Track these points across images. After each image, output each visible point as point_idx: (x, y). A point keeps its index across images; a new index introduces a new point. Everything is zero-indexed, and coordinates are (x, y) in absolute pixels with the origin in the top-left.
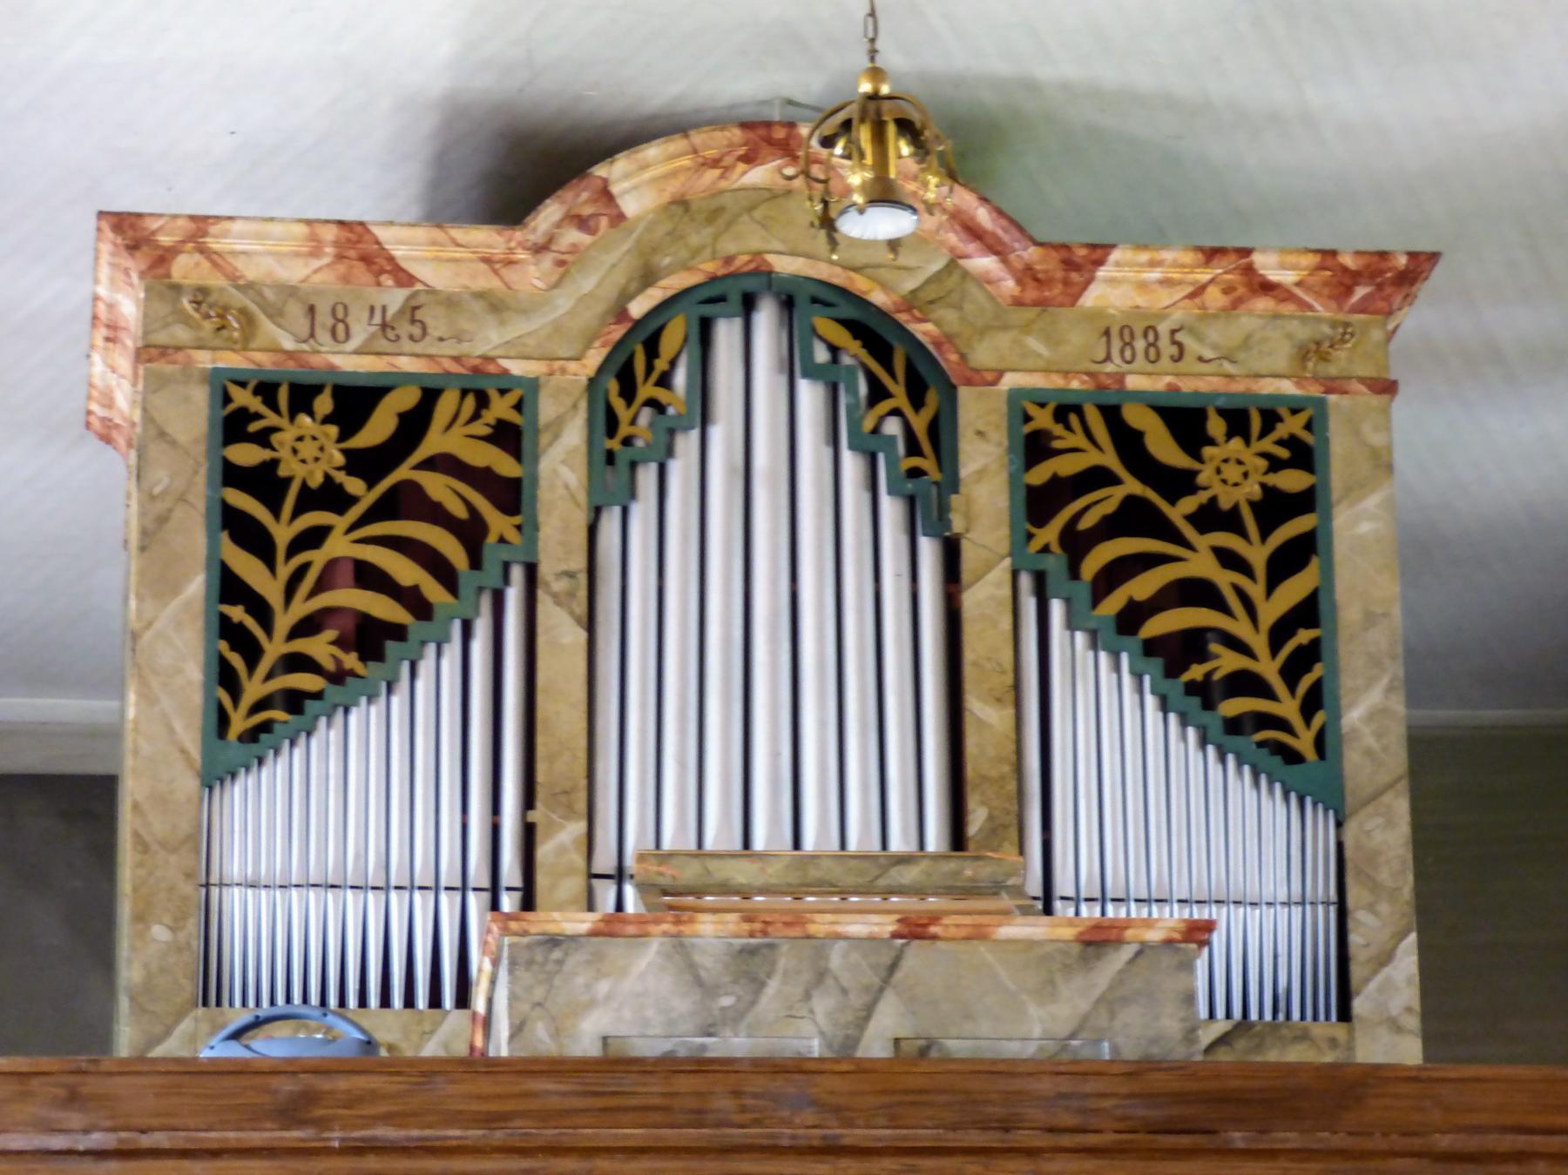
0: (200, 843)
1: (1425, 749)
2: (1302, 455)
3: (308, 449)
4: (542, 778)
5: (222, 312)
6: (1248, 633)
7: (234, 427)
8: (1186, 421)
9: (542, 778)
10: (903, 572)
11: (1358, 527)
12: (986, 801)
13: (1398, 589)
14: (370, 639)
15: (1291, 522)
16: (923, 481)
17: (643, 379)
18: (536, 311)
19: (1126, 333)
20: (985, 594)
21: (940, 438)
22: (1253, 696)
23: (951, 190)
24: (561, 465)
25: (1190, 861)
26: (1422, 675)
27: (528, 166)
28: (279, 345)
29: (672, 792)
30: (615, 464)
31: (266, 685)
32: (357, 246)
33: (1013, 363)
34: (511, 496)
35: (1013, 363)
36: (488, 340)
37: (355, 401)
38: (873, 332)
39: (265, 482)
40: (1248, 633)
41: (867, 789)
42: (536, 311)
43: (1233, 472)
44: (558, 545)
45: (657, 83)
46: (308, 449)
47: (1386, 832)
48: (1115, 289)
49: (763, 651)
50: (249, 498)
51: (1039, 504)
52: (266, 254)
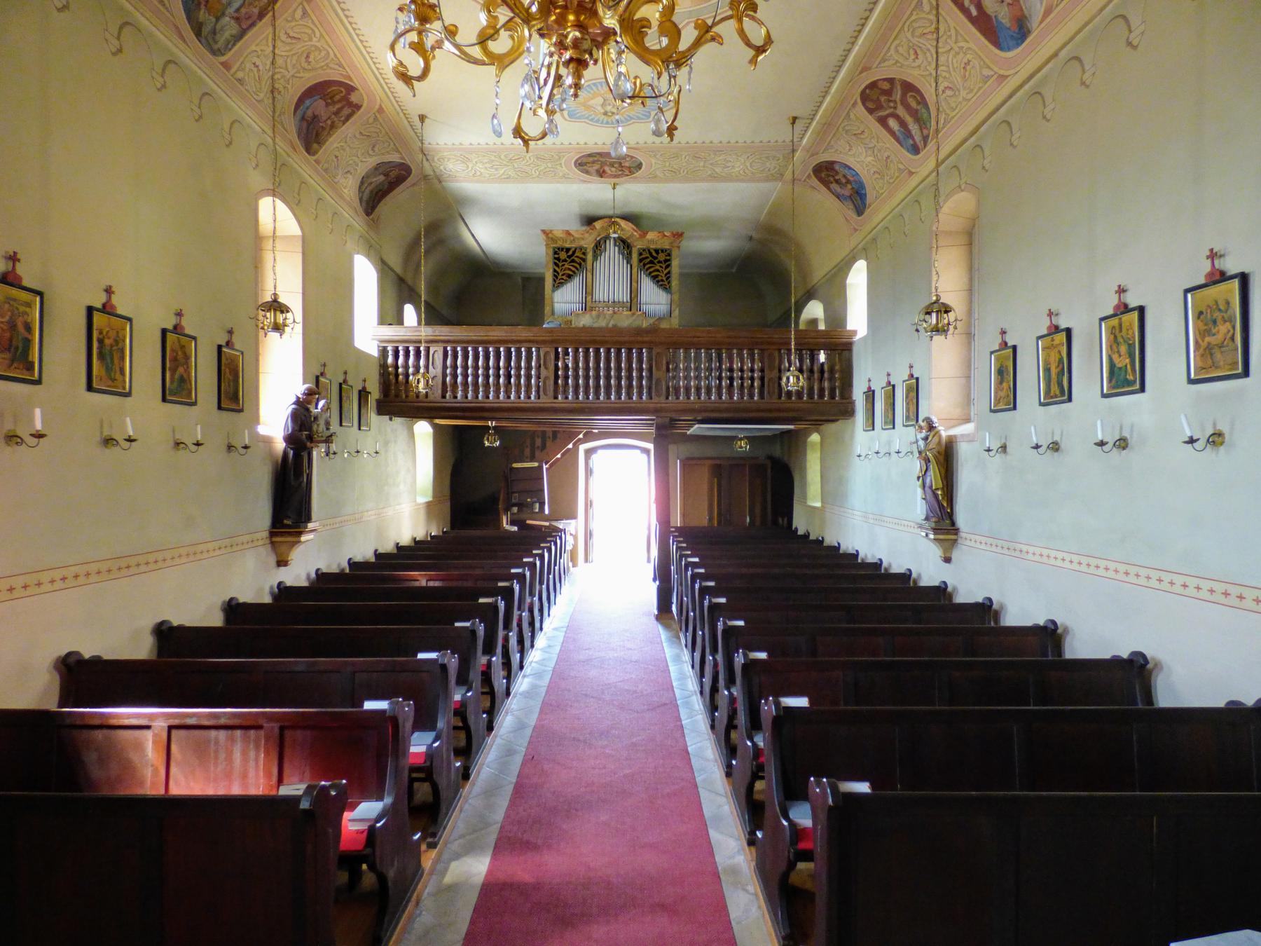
0: (552, 299)
1: (681, 275)
2: (669, 255)
3: (563, 255)
4: (588, 291)
5: (554, 240)
6: (662, 276)
7: (555, 253)
8: (657, 251)
9: (588, 291)
10: (625, 268)
11: (675, 263)
12: (634, 293)
13: (613, 679)
14: (570, 276)
15: (667, 263)
16: (628, 259)
17: (599, 247)
18: (588, 242)
19: (652, 241)
20: (635, 270)
21: (630, 254)
22: (663, 282)
23: (672, 77)
24: (590, 257)
25: (654, 299)
26: (681, 267)
27: (589, 220)
28: (560, 244)
29: (601, 294)
30: (595, 257)
31: (559, 282)
32: (568, 233)
33: (638, 245)
34: (584, 260)
35: (638, 245)
36: (583, 243)
37: (568, 250)
38: (623, 241)
39: (558, 259)
40: (662, 276)
41: (622, 295)
42: (588, 242)
43: (662, 257)
44: (589, 267)
45: (602, 212)
46: (563, 255)
47: (676, 297)
48: (650, 236)
49: (611, 278)
50: (557, 261)
51: (640, 261)
52: (559, 234)
